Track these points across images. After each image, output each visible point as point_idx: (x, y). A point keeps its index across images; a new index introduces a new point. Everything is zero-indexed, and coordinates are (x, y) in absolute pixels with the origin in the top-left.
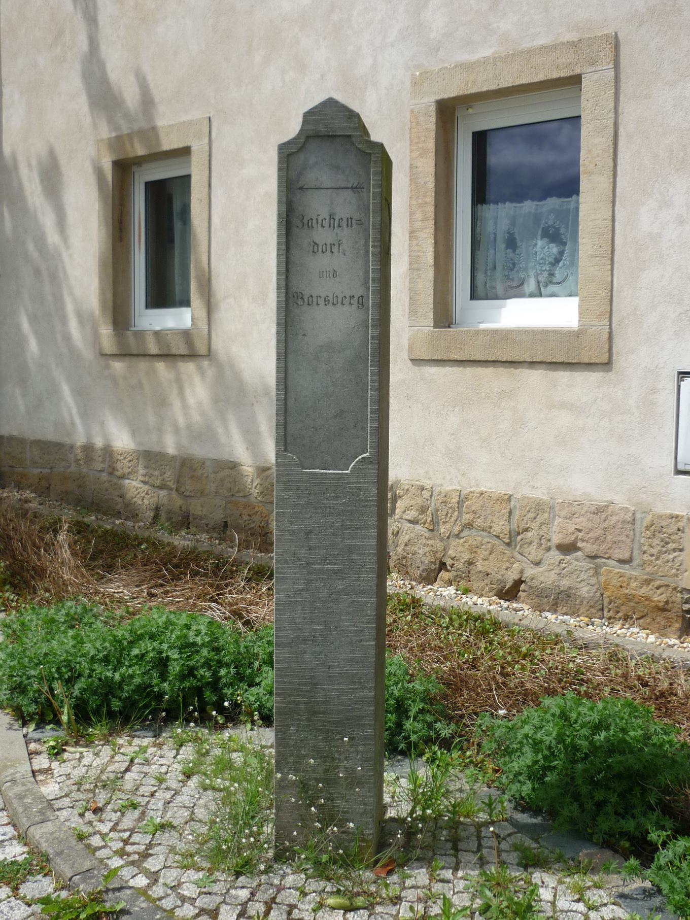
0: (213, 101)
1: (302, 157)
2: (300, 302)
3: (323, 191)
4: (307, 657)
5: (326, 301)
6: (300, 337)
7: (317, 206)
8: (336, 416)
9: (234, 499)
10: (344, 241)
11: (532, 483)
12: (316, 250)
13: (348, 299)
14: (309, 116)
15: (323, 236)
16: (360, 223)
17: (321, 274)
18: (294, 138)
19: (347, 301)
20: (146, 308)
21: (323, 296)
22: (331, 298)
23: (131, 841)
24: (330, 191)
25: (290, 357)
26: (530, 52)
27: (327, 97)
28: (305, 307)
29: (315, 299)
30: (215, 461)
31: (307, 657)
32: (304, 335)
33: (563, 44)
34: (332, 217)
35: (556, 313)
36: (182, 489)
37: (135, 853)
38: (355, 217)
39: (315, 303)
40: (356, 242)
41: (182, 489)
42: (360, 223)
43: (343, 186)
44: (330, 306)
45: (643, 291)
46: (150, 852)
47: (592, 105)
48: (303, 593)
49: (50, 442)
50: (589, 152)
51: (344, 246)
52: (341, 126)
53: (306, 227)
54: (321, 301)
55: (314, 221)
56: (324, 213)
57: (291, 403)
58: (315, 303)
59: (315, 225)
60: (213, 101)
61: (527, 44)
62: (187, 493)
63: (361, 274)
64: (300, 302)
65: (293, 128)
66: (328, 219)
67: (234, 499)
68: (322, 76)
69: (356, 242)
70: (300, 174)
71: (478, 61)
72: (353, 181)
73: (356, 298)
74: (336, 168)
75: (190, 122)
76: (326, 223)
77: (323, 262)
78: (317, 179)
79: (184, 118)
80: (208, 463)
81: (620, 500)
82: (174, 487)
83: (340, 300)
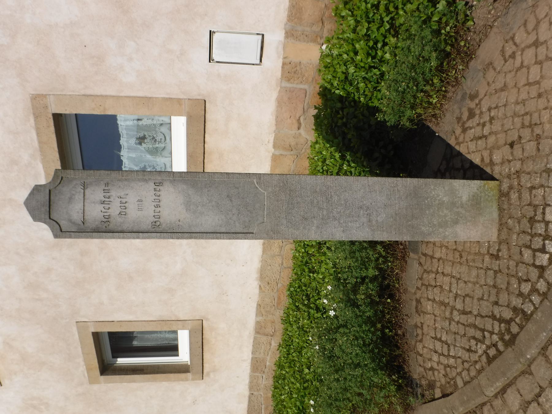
0: (68, 320)
1: (63, 223)
2: (158, 223)
3: (86, 208)
4: (380, 219)
5: (158, 206)
6: (180, 223)
7: (95, 213)
8: (231, 201)
9: (275, 305)
10: (119, 194)
11: (267, 143)
12: (124, 213)
13: (156, 192)
14: (36, 218)
15: (115, 210)
16: (107, 184)
17: (140, 209)
18: (50, 227)
19: (158, 193)
20: (178, 355)
21: (154, 208)
22: (156, 203)
23: (491, 329)
24: (86, 204)
25: (193, 230)
26: (40, 142)
27: (24, 206)
28: (161, 220)
29: (156, 214)
30: (256, 315)
31: (380, 219)
32: (179, 221)
33: (36, 124)
34: (103, 202)
35: (179, 126)
36: (271, 333)
37: (500, 326)
38: (103, 187)
39: (159, 214)
40: (120, 187)
41: (271, 333)
42: (107, 184)
43: (83, 195)
44: (161, 204)
45: (168, 82)
46: (498, 317)
47: (67, 109)
48: (342, 222)
49: (248, 406)
50: (94, 109)
51: (122, 194)
52: (43, 197)
53: (109, 219)
54: (158, 210)
55: (105, 214)
56: (101, 207)
57: (223, 230)
58: (159, 214)
59: (108, 214)
60: (68, 320)
61: (36, 144)
62: (273, 331)
63: (140, 184)
64: (158, 223)
65: (44, 231)
66: (103, 205)
67: (275, 305)
68: (53, 259)
69: (120, 187)
70: (74, 223)
71: (45, 172)
72: (80, 189)
73: (156, 187)
74: (71, 200)
75: (79, 333)
76: (107, 206)
77: (133, 213)
78: (78, 212)
79: (77, 336)
80: (258, 319)
81: (274, 95)
82: (270, 337)
83: (157, 198)
